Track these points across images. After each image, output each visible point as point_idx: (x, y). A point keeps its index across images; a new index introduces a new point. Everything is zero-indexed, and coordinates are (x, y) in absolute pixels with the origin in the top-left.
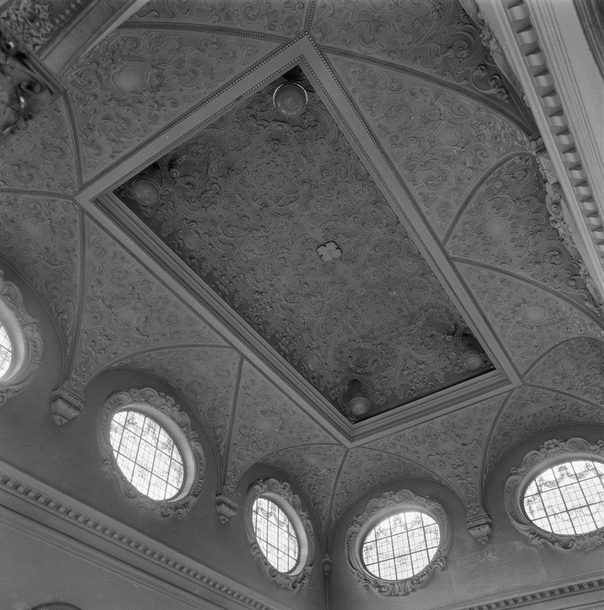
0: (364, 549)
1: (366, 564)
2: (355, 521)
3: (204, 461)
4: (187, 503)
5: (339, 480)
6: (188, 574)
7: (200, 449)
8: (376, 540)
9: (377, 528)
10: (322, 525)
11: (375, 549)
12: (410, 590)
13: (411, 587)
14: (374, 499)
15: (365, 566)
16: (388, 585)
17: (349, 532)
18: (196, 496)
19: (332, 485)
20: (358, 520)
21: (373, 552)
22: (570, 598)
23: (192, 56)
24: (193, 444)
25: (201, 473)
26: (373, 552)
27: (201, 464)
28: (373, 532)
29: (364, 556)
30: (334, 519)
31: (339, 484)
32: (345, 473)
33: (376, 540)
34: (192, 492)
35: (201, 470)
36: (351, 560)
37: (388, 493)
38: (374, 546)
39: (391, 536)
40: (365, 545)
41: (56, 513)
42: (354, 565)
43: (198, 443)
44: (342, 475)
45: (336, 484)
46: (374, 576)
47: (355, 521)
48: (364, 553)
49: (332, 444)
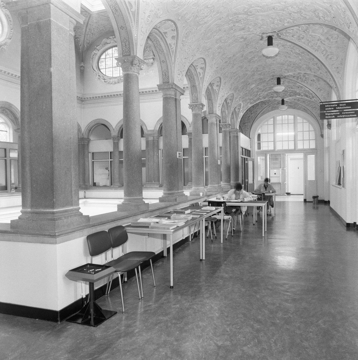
0: (100, 62)
1: (100, 68)
2: (96, 48)
3: (11, 19)
4: (6, 43)
5: (88, 28)
6: (16, 77)
7: (8, 13)
8: (105, 58)
9: (106, 52)
10: (80, 49)
11: (105, 63)
12: (117, 82)
13: (117, 81)
14: (105, 39)
15: (99, 69)
16: (108, 79)
17: (93, 54)
18: (10, 39)
19: (84, 30)
20: (97, 48)
21: (104, 64)
22: (114, 98)
23: (101, 121)
24: (4, 10)
25: (11, 26)
26: (104, 64)
27: (10, 21)
28: (104, 54)
29: (100, 65)
30: (86, 46)
31: (88, 30)
32: (90, 25)
33: (105, 58)
34: (8, 37)
35: (11, 24)
36: (93, 67)
37: (112, 37)
38: (104, 61)
39: (112, 57)
40: (100, 60)
41: (15, 78)
42: (94, 69)
43: (6, 9)
44: (89, 26)
45: (86, 30)
46: (103, 74)
47: (96, 48)
48: (99, 63)
49: (83, 11)
